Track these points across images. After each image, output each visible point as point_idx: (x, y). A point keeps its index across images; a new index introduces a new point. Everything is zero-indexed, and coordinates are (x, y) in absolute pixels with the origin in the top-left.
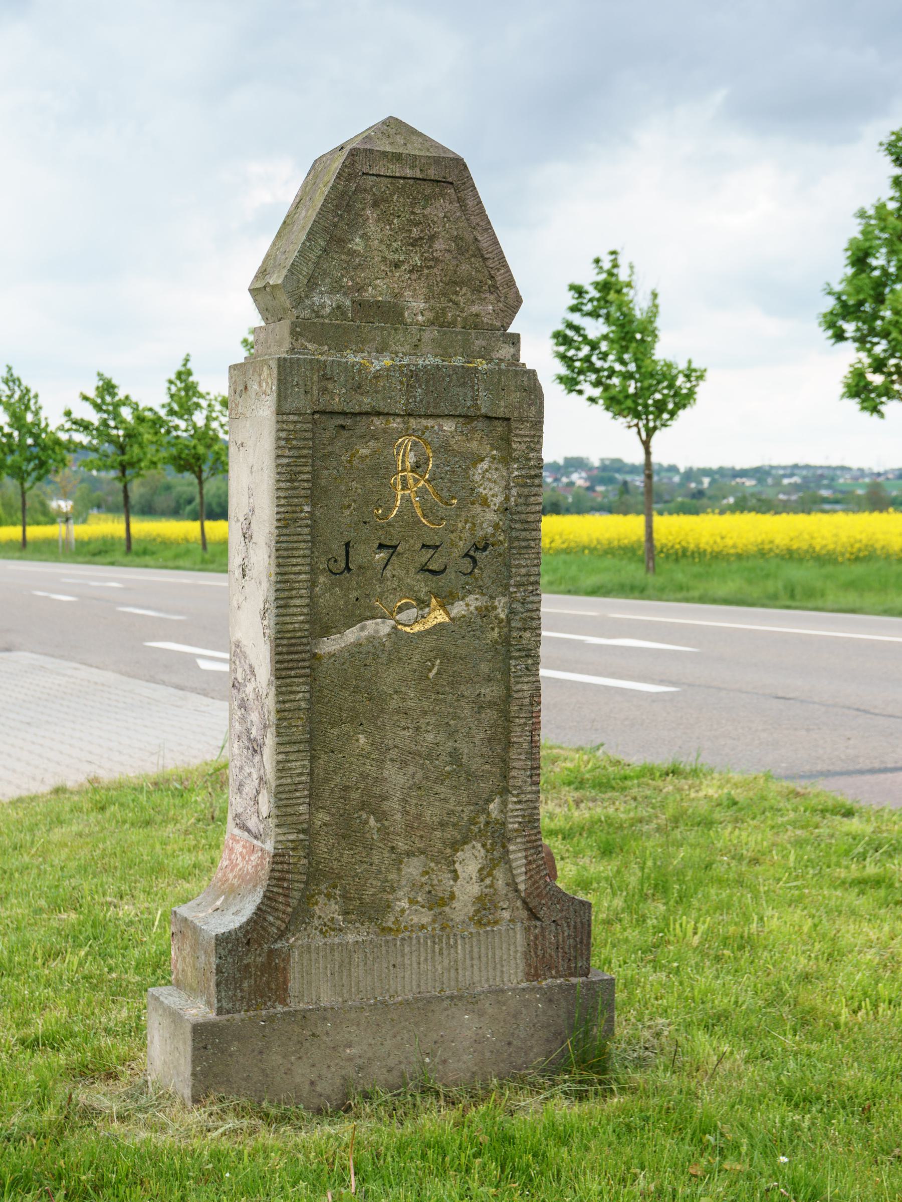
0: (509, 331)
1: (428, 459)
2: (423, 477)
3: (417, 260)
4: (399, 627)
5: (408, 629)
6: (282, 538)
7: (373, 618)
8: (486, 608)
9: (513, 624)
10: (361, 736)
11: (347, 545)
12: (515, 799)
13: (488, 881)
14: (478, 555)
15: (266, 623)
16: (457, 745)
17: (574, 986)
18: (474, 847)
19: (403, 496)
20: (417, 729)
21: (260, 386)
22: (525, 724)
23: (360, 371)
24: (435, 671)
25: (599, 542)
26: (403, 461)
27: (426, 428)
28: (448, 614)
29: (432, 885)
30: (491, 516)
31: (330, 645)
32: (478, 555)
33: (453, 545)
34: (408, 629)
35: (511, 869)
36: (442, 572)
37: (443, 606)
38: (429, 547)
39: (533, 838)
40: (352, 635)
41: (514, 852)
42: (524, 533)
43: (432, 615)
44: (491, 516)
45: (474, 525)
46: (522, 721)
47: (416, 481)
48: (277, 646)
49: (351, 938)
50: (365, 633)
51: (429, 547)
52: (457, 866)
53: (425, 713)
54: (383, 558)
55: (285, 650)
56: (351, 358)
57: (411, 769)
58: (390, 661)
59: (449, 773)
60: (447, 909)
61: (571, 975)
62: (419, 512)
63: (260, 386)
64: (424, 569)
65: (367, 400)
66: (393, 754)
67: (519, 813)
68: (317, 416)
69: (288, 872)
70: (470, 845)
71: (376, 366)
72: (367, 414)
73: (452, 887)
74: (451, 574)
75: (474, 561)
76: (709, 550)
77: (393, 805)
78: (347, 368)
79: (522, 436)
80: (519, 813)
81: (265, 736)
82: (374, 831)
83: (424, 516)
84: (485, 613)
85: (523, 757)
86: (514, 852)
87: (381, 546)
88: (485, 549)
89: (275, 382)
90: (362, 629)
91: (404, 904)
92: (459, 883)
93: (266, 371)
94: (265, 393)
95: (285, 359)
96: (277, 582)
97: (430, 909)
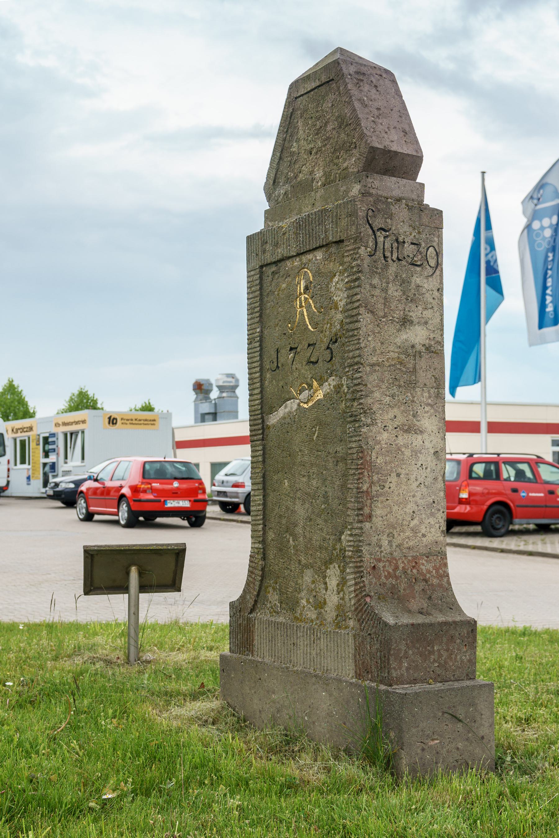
0: (417, 181)
4: (301, 404)
7: (290, 399)
8: (338, 385)
10: (286, 481)
12: (349, 533)
13: (341, 595)
16: (327, 489)
17: (380, 691)
18: (334, 567)
20: (309, 476)
22: (354, 474)
24: (316, 435)
27: (310, 260)
29: (316, 592)
30: (340, 316)
33: (322, 341)
36: (317, 362)
39: (359, 564)
40: (282, 412)
42: (351, 325)
43: (316, 395)
44: (340, 316)
45: (331, 324)
46: (353, 471)
49: (281, 619)
50: (287, 410)
51: (312, 345)
52: (327, 579)
53: (312, 465)
54: (292, 357)
57: (307, 505)
58: (297, 428)
59: (323, 510)
60: (323, 610)
61: (381, 682)
64: (309, 362)
66: (299, 494)
67: (352, 543)
70: (333, 565)
73: (324, 594)
74: (320, 364)
77: (299, 530)
79: (349, 251)
80: (352, 543)
82: (292, 548)
84: (338, 388)
85: (353, 500)
88: (336, 342)
90: (286, 407)
91: (304, 602)
92: (328, 593)
97: (316, 609)
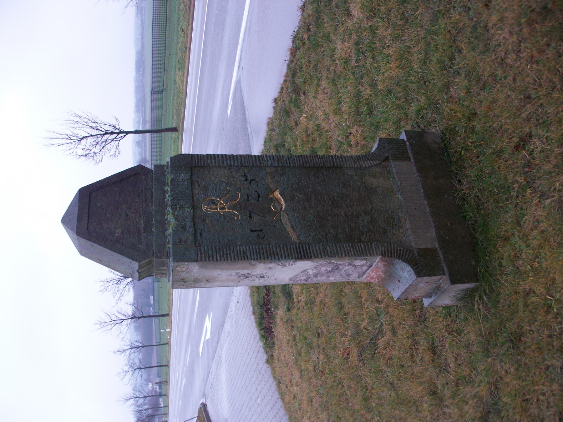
1: (212, 199)
2: (219, 201)
3: (124, 206)
5: (284, 206)
6: (252, 258)
9: (277, 165)
11: (252, 231)
14: (249, 179)
15: (287, 264)
19: (228, 209)
21: (184, 271)
23: (176, 227)
25: (138, 335)
26: (213, 209)
28: (275, 191)
31: (294, 237)
32: (249, 179)
34: (284, 206)
35: (372, 166)
37: (272, 192)
38: (248, 198)
41: (365, 165)
47: (221, 204)
48: (298, 258)
55: (299, 255)
56: (170, 230)
62: (234, 203)
63: (184, 271)
65: (188, 224)
68: (197, 245)
69: (388, 250)
71: (173, 221)
72: (194, 224)
75: (252, 180)
76: (171, 262)
78: (175, 232)
81: (333, 263)
83: (235, 200)
86: (365, 165)
87: (250, 217)
89: (183, 263)
93: (178, 269)
94: (187, 269)
95: (173, 259)
96: (272, 259)
